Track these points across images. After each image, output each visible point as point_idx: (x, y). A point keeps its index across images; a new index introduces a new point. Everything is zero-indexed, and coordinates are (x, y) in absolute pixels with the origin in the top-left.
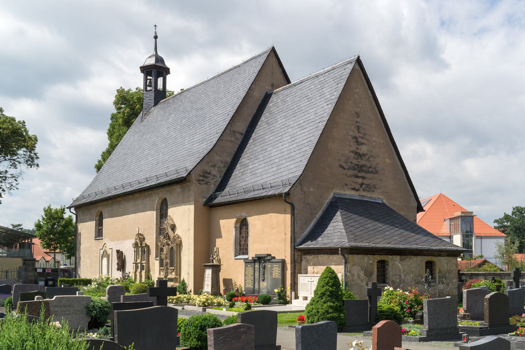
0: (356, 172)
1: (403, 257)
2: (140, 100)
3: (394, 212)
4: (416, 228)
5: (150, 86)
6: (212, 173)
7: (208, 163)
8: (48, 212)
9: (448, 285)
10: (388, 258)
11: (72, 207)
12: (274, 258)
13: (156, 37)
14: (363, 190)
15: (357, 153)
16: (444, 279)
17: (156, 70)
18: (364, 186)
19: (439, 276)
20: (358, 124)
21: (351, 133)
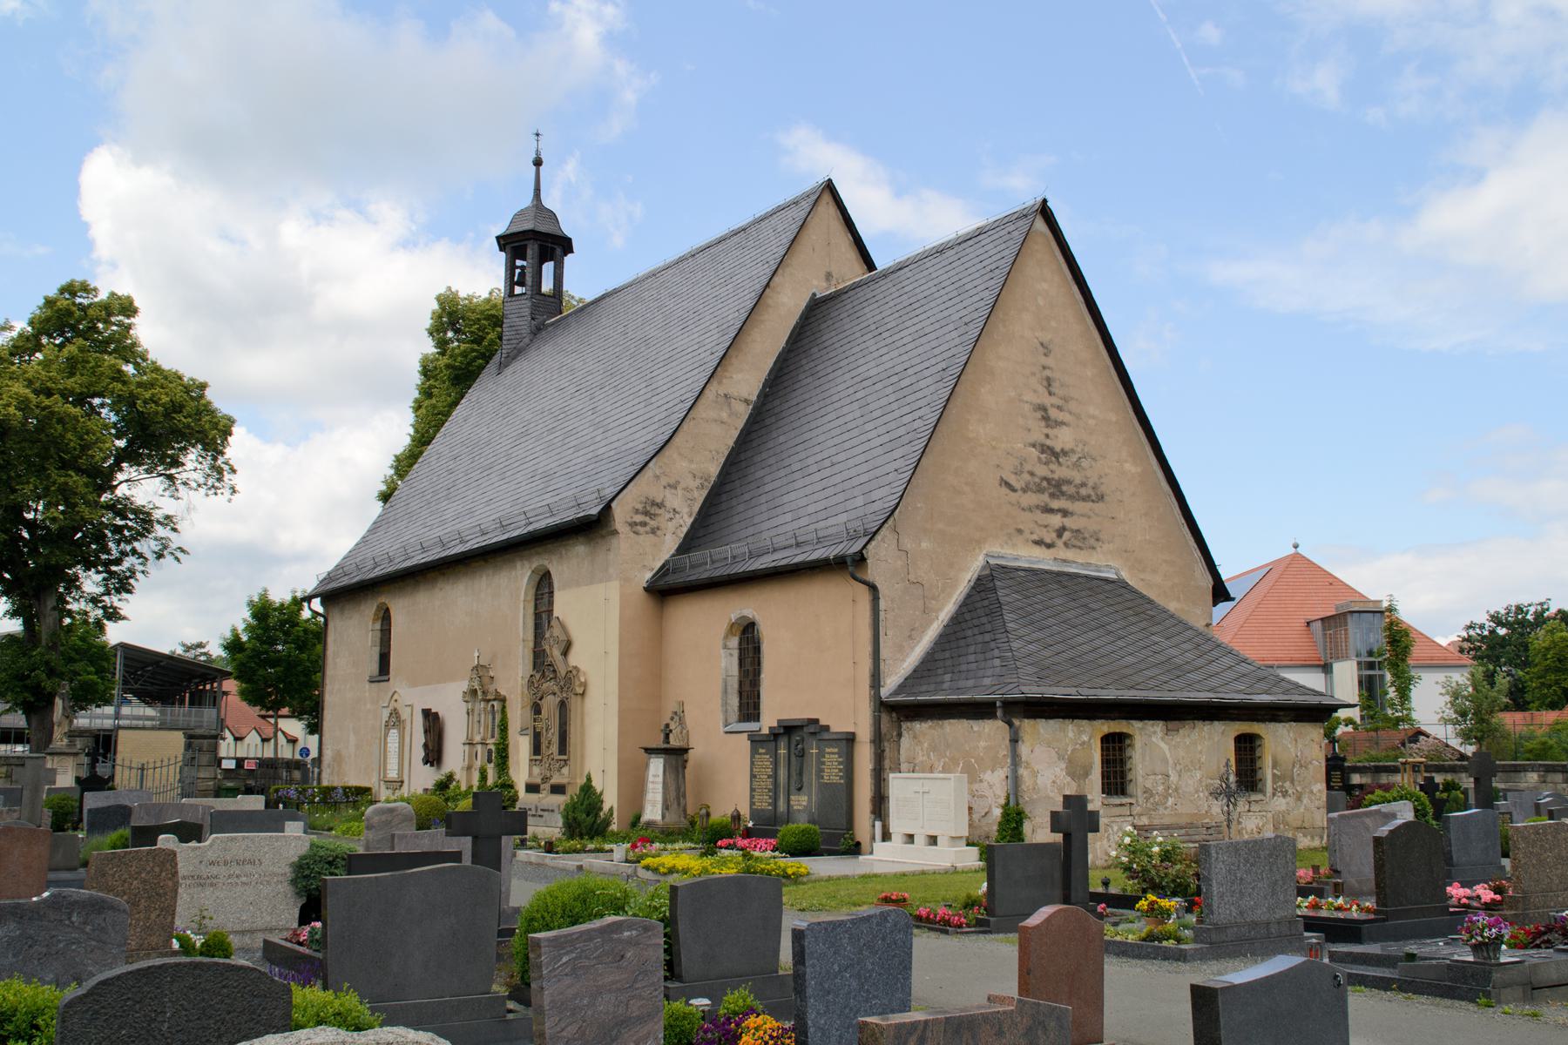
0: (1045, 498)
1: (1171, 724)
2: (497, 321)
3: (1150, 602)
4: (1206, 647)
5: (521, 283)
6: (668, 504)
7: (657, 477)
8: (262, 611)
9: (1299, 799)
10: (1134, 728)
11: (315, 596)
12: (827, 728)
13: (538, 163)
14: (1066, 544)
15: (1045, 449)
16: (1287, 784)
17: (535, 244)
18: (1067, 535)
19: (1274, 775)
20: (1047, 373)
21: (1029, 396)
